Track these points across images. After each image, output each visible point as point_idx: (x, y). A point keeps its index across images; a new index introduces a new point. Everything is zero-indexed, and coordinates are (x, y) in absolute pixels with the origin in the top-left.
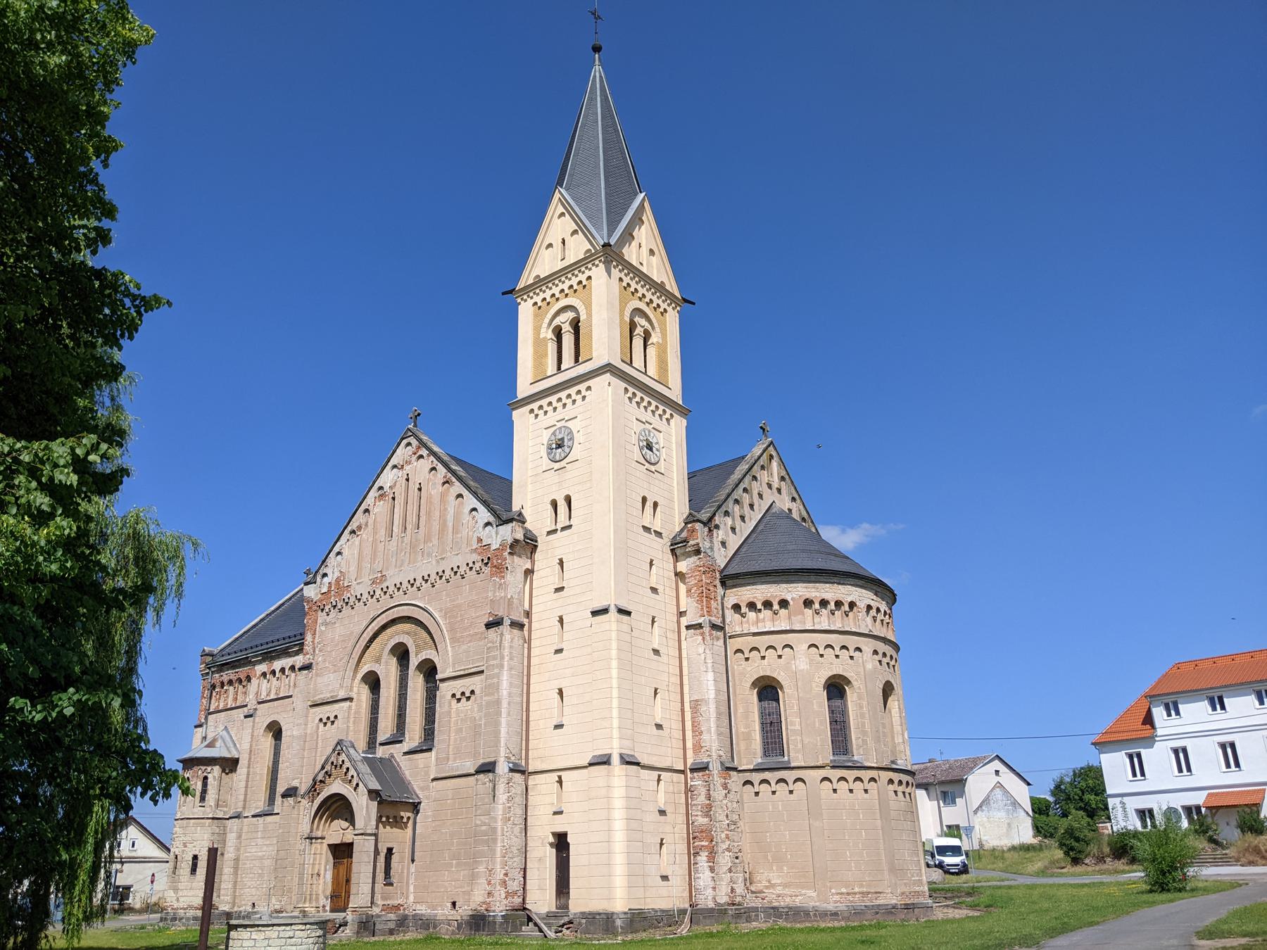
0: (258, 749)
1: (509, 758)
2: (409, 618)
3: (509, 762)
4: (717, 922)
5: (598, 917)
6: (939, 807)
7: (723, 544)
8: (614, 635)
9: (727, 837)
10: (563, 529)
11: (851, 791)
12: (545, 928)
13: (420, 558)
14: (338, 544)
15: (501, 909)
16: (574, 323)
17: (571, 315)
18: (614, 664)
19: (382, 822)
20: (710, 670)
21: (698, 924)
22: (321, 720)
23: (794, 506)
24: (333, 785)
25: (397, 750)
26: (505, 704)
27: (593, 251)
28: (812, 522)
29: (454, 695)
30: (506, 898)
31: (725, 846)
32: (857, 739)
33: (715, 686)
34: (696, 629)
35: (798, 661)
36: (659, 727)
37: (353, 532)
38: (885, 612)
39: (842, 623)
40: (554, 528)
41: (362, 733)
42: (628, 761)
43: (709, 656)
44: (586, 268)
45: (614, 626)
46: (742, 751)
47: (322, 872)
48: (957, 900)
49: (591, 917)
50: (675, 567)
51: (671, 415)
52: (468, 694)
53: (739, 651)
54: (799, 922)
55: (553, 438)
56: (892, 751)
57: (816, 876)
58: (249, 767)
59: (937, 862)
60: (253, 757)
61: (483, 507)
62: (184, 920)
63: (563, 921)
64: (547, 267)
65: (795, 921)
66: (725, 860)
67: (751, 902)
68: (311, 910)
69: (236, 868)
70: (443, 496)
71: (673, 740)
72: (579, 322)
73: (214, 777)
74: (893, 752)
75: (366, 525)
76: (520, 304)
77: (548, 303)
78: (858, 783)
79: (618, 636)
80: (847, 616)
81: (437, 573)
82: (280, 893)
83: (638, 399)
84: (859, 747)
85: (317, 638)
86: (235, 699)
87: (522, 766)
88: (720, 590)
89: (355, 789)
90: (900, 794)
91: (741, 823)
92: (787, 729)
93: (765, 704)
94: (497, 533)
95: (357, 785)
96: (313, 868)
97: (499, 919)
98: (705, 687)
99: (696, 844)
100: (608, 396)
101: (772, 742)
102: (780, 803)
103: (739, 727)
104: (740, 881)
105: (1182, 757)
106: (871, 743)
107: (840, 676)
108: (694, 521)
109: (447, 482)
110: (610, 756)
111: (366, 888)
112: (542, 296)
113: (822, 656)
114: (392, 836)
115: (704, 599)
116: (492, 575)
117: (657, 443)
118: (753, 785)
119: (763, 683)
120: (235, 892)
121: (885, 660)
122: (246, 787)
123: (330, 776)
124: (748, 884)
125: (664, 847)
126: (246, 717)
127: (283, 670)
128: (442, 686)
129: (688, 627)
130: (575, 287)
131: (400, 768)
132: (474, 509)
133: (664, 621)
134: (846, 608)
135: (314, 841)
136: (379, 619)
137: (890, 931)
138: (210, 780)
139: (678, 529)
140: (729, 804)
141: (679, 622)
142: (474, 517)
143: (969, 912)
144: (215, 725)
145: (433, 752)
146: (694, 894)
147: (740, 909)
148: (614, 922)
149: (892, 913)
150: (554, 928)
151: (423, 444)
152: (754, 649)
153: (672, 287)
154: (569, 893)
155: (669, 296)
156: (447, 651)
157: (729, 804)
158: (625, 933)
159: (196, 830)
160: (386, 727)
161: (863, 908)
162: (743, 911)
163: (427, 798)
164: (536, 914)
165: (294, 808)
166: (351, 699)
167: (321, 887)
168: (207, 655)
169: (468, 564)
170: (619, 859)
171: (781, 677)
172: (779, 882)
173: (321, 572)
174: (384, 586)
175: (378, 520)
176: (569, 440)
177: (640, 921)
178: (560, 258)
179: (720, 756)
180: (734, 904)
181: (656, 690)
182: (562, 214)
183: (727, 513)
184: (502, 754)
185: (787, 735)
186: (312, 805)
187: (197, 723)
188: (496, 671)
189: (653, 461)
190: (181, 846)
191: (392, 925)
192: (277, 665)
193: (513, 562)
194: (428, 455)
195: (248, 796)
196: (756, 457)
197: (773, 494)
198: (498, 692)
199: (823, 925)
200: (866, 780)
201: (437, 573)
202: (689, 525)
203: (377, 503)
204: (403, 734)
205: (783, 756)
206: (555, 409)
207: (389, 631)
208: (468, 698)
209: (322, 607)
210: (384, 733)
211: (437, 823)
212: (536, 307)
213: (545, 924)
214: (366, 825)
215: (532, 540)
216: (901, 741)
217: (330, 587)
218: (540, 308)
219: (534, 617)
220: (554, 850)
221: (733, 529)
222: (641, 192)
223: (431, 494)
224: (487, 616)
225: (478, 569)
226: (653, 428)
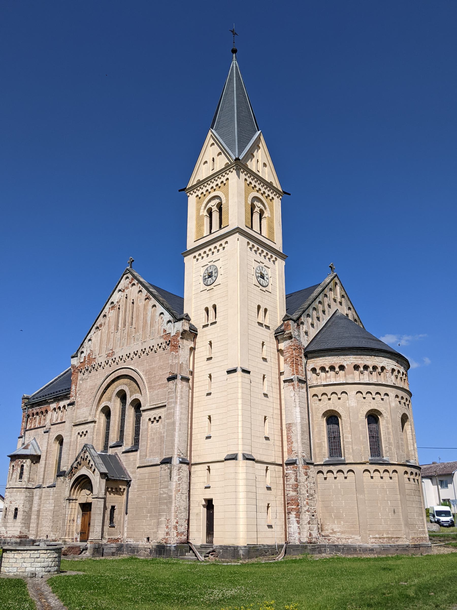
0: (51, 450)
1: (180, 456)
2: (127, 375)
3: (179, 458)
4: (301, 554)
5: (229, 549)
6: (438, 489)
7: (306, 333)
8: (240, 385)
9: (307, 503)
10: (212, 324)
11: (382, 478)
12: (198, 554)
13: (133, 342)
14: (90, 335)
15: (174, 542)
16: (219, 207)
17: (217, 201)
18: (240, 401)
19: (109, 491)
20: (298, 406)
21: (290, 554)
22: (79, 433)
23: (349, 313)
24: (82, 470)
25: (119, 451)
26: (177, 424)
27: (230, 164)
28: (361, 322)
29: (150, 419)
30: (177, 536)
31: (306, 509)
32: (386, 447)
33: (301, 415)
34: (289, 382)
35: (350, 402)
36: (267, 438)
37: (97, 328)
38: (403, 373)
39: (377, 379)
40: (207, 323)
41: (101, 441)
42: (247, 458)
43: (297, 398)
44: (226, 173)
45: (240, 380)
46: (317, 453)
47: (76, 519)
48: (447, 542)
49: (225, 548)
50: (278, 346)
51: (276, 258)
52: (157, 419)
53: (315, 395)
54: (350, 554)
55: (206, 272)
56: (407, 455)
57: (361, 527)
58: (46, 460)
59: (436, 520)
60: (48, 454)
61: (166, 312)
62: (10, 544)
63: (209, 551)
64: (204, 175)
65: (348, 554)
66: (306, 517)
67: (322, 542)
68: (69, 541)
69: (38, 516)
70: (145, 306)
71: (275, 446)
72: (222, 205)
73: (27, 465)
74: (408, 455)
75: (105, 324)
76: (189, 196)
77: (205, 195)
78: (386, 473)
79: (242, 385)
80: (380, 375)
81: (142, 350)
82: (55, 530)
83: (255, 249)
84: (387, 452)
85: (78, 387)
86: (40, 423)
87: (187, 460)
88: (304, 360)
89: (93, 472)
90: (412, 480)
91: (316, 496)
92: (343, 441)
93: (331, 426)
94: (174, 327)
95: (94, 470)
96: (70, 517)
97: (173, 548)
98: (295, 416)
99: (289, 507)
100: (237, 247)
101: (334, 449)
102: (339, 484)
103: (315, 440)
104: (315, 530)
106: (394, 449)
107: (376, 410)
108: (288, 320)
109: (148, 298)
110: (237, 454)
111: (99, 529)
112: (201, 191)
113: (364, 398)
114: (113, 499)
115: (294, 365)
116: (171, 350)
117: (267, 275)
118: (323, 473)
119: (329, 414)
120: (37, 529)
121: (403, 401)
122: (44, 471)
123: (80, 464)
124: (320, 531)
125: (270, 509)
126: (45, 432)
127: (64, 407)
128: (144, 414)
129: (285, 381)
130: (220, 185)
131: (121, 461)
132: (162, 313)
133: (272, 376)
134: (379, 370)
135: (71, 501)
136: (110, 376)
137: (403, 562)
138: (25, 467)
139: (279, 325)
140: (309, 484)
141: (279, 379)
142: (162, 318)
143: (453, 549)
144: (29, 437)
145: (138, 452)
146: (288, 537)
147: (315, 546)
148: (238, 552)
149: (406, 550)
150: (203, 555)
151: (135, 277)
152: (324, 394)
153: (280, 189)
154: (213, 534)
155: (275, 190)
156: (147, 394)
157: (309, 484)
158: (244, 559)
159: (17, 494)
160: (114, 438)
161: (389, 546)
162: (316, 547)
163: (135, 478)
164: (194, 546)
165: (63, 482)
166: (94, 422)
167: (75, 528)
168: (25, 398)
169: (158, 345)
170: (242, 515)
171: (340, 410)
173: (80, 351)
174: (113, 358)
175: (111, 320)
176: (215, 273)
177: (254, 552)
178: (211, 169)
179: (303, 456)
180: (311, 543)
181: (265, 417)
182: (213, 144)
183: (308, 316)
184: (176, 453)
185: (344, 444)
186: (70, 481)
187: (20, 436)
188: (173, 405)
189: (264, 285)
190: (9, 503)
191: (113, 550)
192: (62, 404)
193: (183, 343)
194: (138, 284)
195: (45, 476)
196: (327, 284)
197: (337, 305)
198: (174, 417)
199: (364, 556)
200: (391, 472)
201: (142, 350)
202: (286, 322)
203: (110, 311)
204: (123, 441)
205: (341, 456)
206: (208, 255)
207: (116, 383)
208: (158, 421)
209: (80, 370)
210: (113, 441)
211: (140, 492)
212: (198, 198)
213: (199, 552)
214: (99, 493)
215: (194, 331)
216: (412, 449)
217: (85, 359)
218: (200, 198)
219: (195, 375)
220: (205, 509)
221: (312, 325)
222: (259, 130)
223: (139, 305)
224: (168, 374)
225: (164, 347)
226: (265, 266)
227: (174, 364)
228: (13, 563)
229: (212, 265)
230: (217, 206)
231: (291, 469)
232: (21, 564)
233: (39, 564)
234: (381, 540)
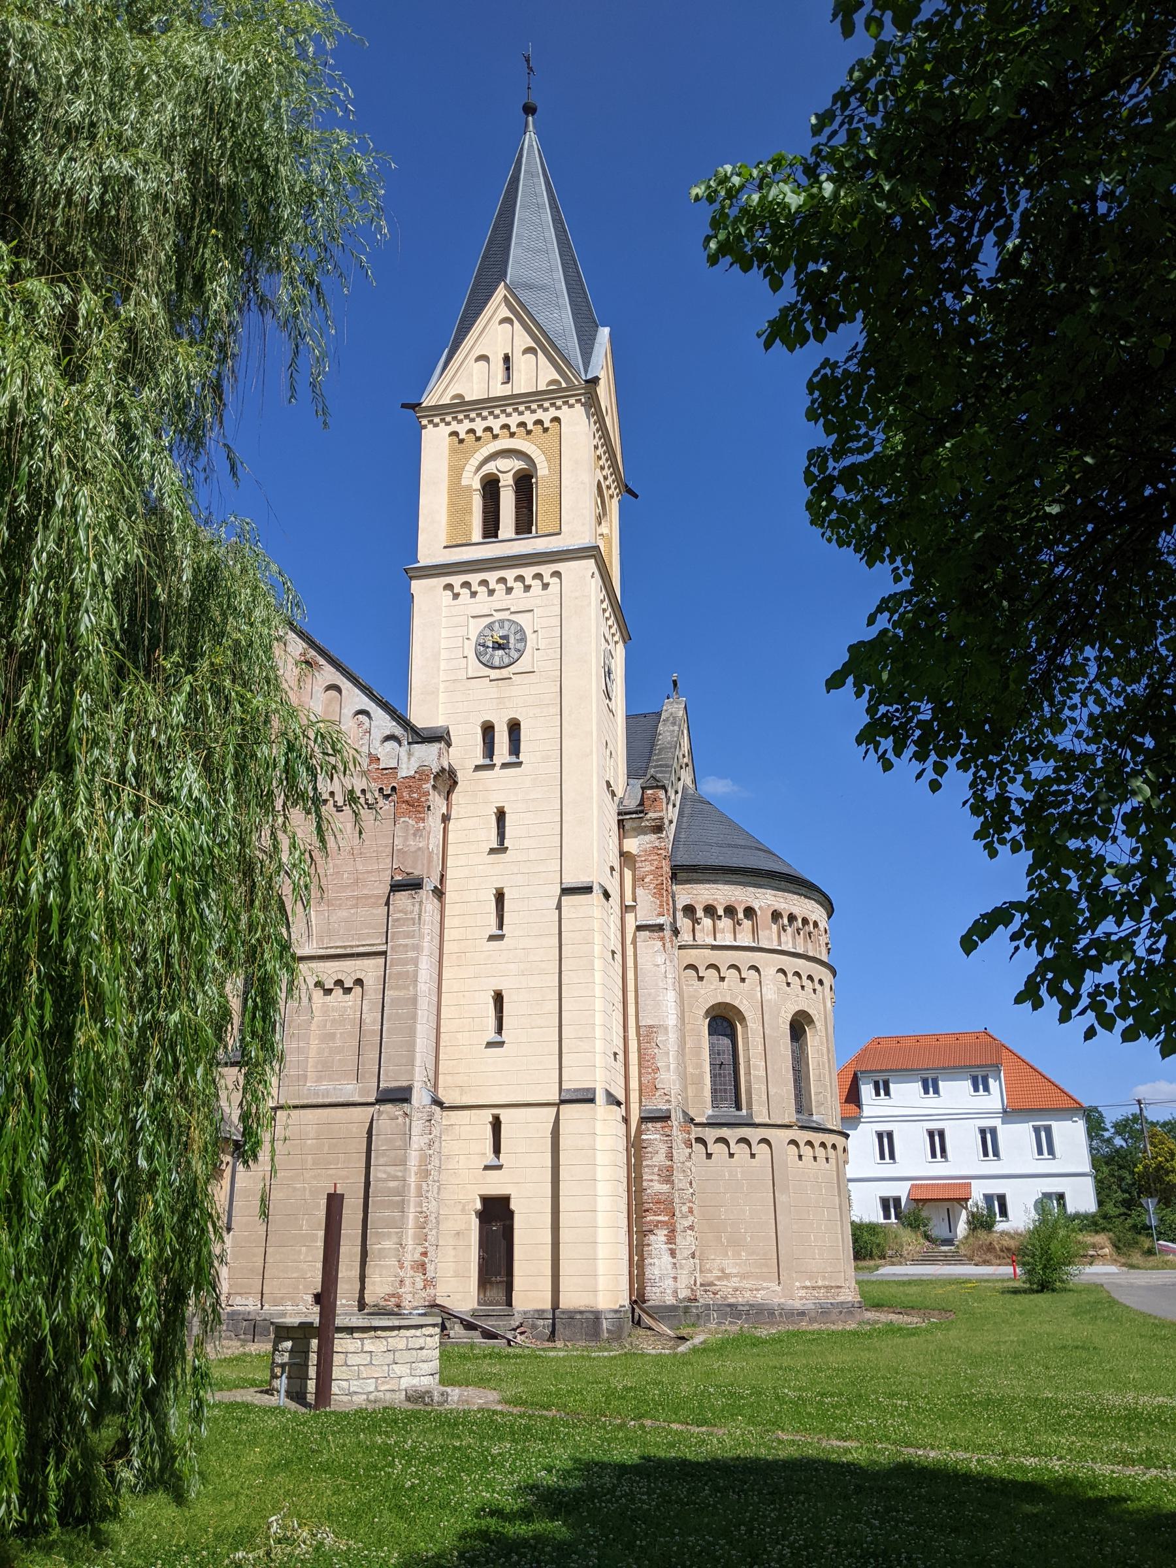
29: (319, 984)
34: (653, 931)
50: (621, 844)
76: (425, 427)
105: (886, 1144)
108: (657, 787)
119: (718, 1012)
172: (735, 1271)
188: (411, 954)
227: (413, 849)
228: (362, 1368)
229: (508, 620)
230: (514, 475)
231: (656, 1131)
232: (386, 1368)
233: (424, 1366)
234: (815, 1293)
